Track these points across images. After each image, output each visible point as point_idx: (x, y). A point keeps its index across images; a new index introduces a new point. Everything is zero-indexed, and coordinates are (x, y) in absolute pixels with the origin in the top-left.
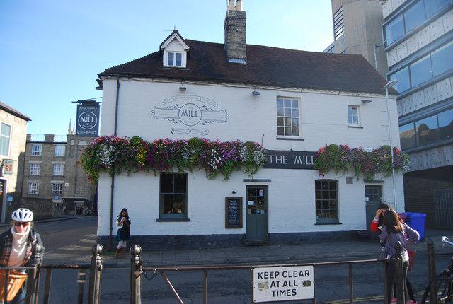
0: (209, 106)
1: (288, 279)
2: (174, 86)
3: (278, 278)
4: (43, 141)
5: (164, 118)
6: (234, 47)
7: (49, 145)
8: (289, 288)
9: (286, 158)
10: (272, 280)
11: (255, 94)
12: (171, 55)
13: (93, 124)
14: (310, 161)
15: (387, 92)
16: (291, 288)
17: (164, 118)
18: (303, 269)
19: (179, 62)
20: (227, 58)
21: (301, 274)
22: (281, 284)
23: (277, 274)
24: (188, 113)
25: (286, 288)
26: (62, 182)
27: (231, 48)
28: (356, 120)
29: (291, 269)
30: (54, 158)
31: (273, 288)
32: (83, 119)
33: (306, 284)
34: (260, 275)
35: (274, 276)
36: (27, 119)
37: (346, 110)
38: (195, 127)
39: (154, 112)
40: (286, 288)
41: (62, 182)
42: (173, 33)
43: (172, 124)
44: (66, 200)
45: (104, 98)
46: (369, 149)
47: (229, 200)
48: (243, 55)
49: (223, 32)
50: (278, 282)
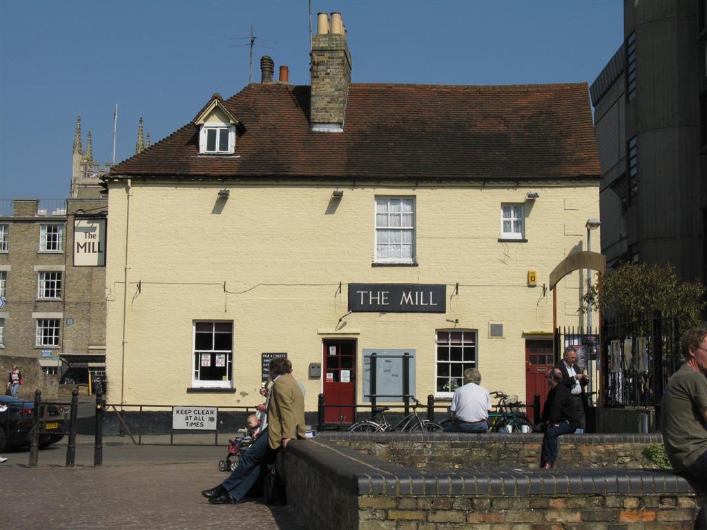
3: (190, 414)
4: (96, 264)
8: (198, 421)
12: (212, 134)
14: (426, 299)
16: (200, 422)
19: (224, 145)
20: (311, 123)
21: (208, 413)
22: (193, 418)
25: (196, 421)
27: (317, 105)
31: (187, 421)
33: (212, 419)
34: (177, 412)
40: (196, 421)
44: (70, 359)
50: (191, 417)
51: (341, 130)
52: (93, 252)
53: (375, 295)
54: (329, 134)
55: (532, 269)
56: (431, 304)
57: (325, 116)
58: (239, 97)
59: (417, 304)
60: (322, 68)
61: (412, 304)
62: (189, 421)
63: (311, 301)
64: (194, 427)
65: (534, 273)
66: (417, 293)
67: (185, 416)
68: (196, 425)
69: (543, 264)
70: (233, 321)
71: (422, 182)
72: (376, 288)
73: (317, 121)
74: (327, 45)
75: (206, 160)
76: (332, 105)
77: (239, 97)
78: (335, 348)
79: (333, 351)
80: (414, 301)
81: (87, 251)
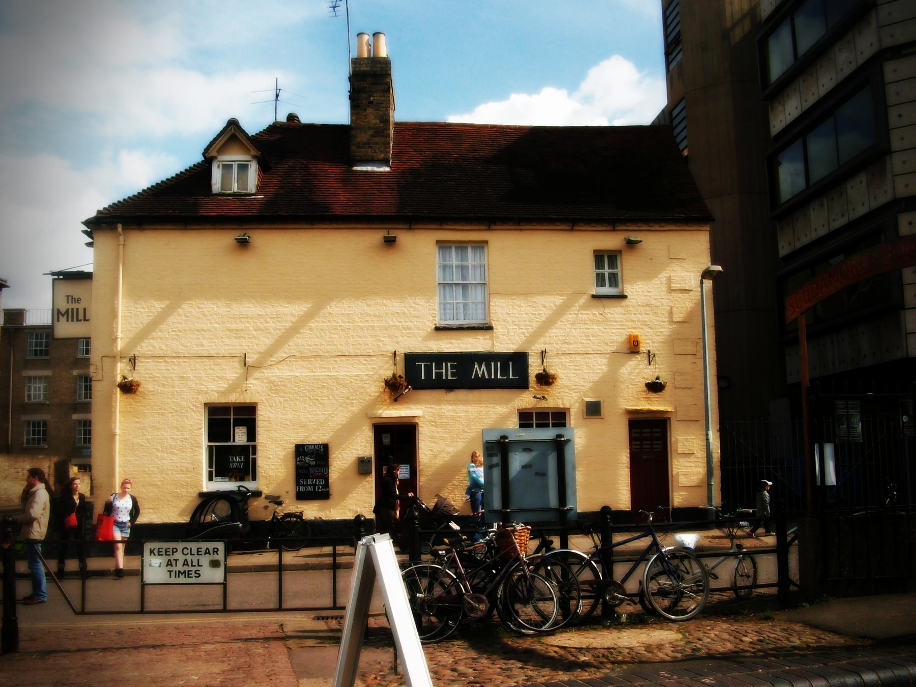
1: (189, 558)
6: (363, 137)
8: (190, 568)
10: (168, 557)
11: (390, 242)
14: (505, 371)
16: (194, 569)
18: (211, 545)
21: (207, 552)
22: (180, 563)
23: (175, 551)
27: (358, 140)
28: (614, 280)
29: (194, 546)
31: (169, 568)
34: (152, 552)
35: (171, 553)
36: (44, 274)
37: (590, 261)
40: (186, 568)
45: (97, 263)
47: (300, 450)
50: (176, 560)
51: (387, 169)
52: (78, 320)
53: (439, 367)
54: (373, 172)
55: (635, 332)
56: (511, 377)
57: (367, 152)
58: (262, 136)
59: (493, 377)
60: (364, 95)
61: (487, 377)
62: (174, 568)
63: (357, 376)
64: (182, 579)
65: (637, 336)
66: (492, 364)
67: (166, 558)
68: (187, 574)
69: (646, 325)
70: (256, 403)
71: (495, 224)
72: (440, 358)
73: (358, 158)
74: (369, 69)
76: (376, 140)
77: (262, 136)
78: (389, 435)
79: (386, 440)
80: (490, 374)
81: (70, 319)
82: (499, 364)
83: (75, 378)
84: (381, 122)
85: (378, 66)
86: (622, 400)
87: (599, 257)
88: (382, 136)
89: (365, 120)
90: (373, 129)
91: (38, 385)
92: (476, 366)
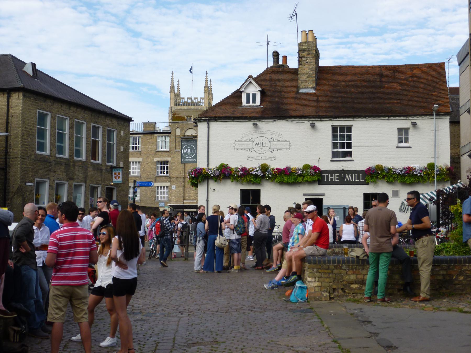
0: (275, 138)
2: (247, 126)
5: (242, 149)
7: (149, 137)
9: (337, 176)
12: (248, 96)
13: (193, 154)
14: (359, 178)
15: (434, 114)
17: (242, 149)
19: (254, 101)
20: (299, 88)
24: (260, 144)
26: (168, 184)
27: (301, 79)
30: (156, 152)
32: (186, 151)
37: (396, 133)
38: (265, 155)
39: (234, 145)
41: (168, 184)
42: (248, 78)
43: (248, 153)
46: (365, 169)
48: (313, 85)
49: (297, 62)
53: (332, 176)
56: (361, 180)
61: (351, 180)
72: (332, 173)
75: (246, 109)
76: (309, 79)
82: (356, 175)
83: (155, 162)
84: (311, 71)
85: (310, 46)
86: (251, 257)
87: (400, 130)
88: (312, 77)
89: (304, 70)
90: (308, 74)
91: (134, 166)
92: (347, 176)
